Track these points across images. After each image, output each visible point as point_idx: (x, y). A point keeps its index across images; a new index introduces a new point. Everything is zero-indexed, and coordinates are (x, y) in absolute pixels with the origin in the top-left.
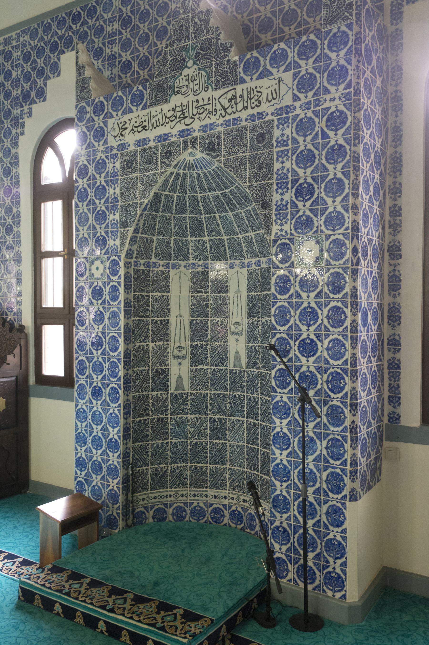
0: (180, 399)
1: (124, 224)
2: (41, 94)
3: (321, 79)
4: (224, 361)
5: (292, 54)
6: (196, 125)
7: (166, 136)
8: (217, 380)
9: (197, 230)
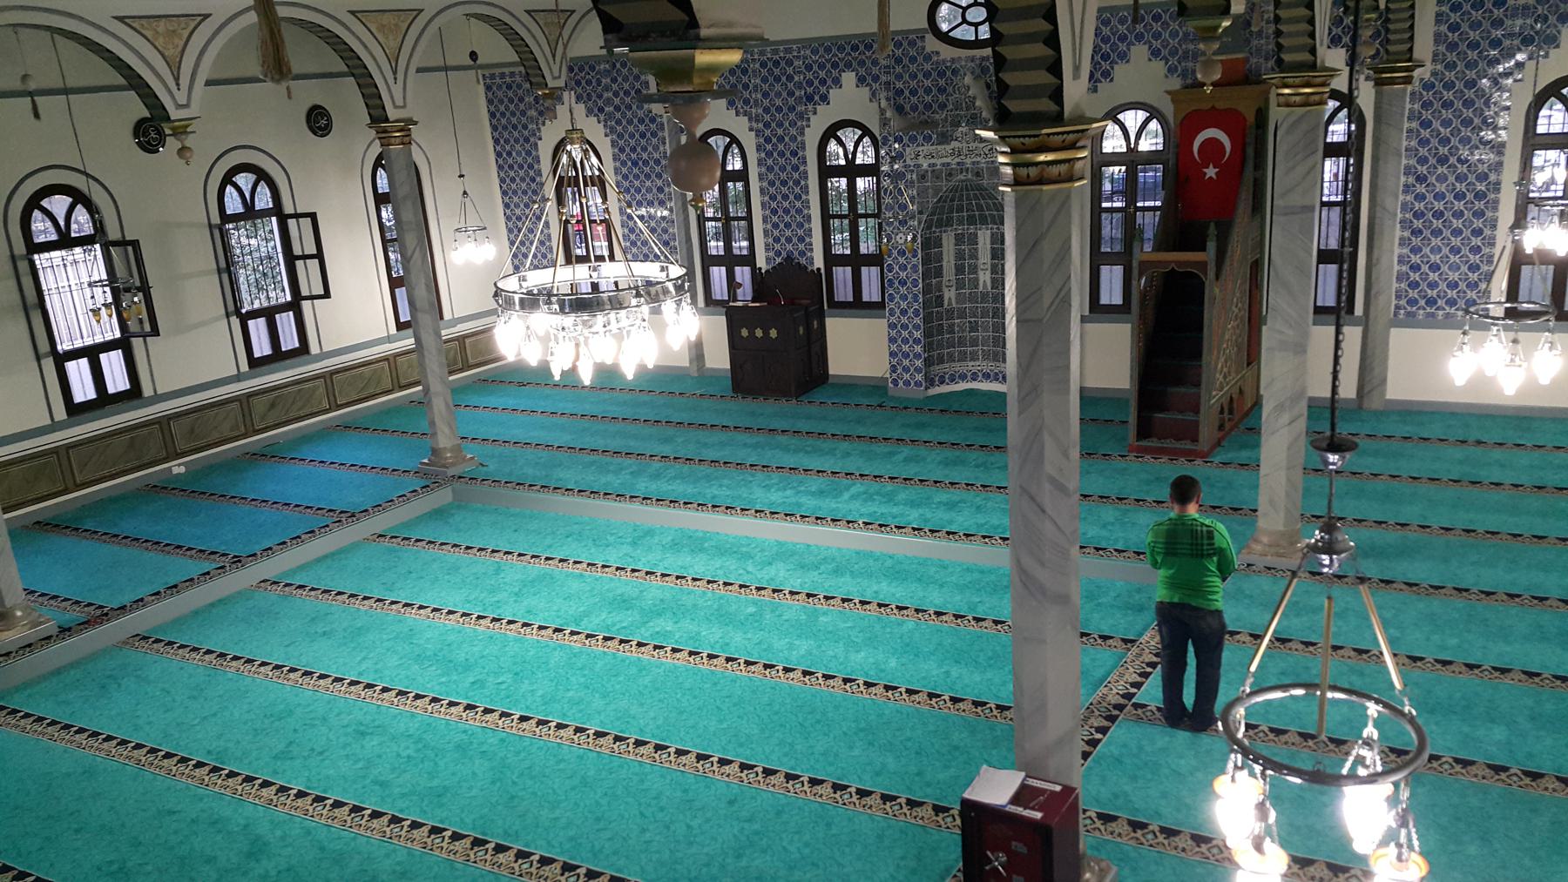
0: (950, 312)
1: (920, 213)
2: (825, 99)
6: (968, 161)
8: (972, 298)
9: (960, 209)
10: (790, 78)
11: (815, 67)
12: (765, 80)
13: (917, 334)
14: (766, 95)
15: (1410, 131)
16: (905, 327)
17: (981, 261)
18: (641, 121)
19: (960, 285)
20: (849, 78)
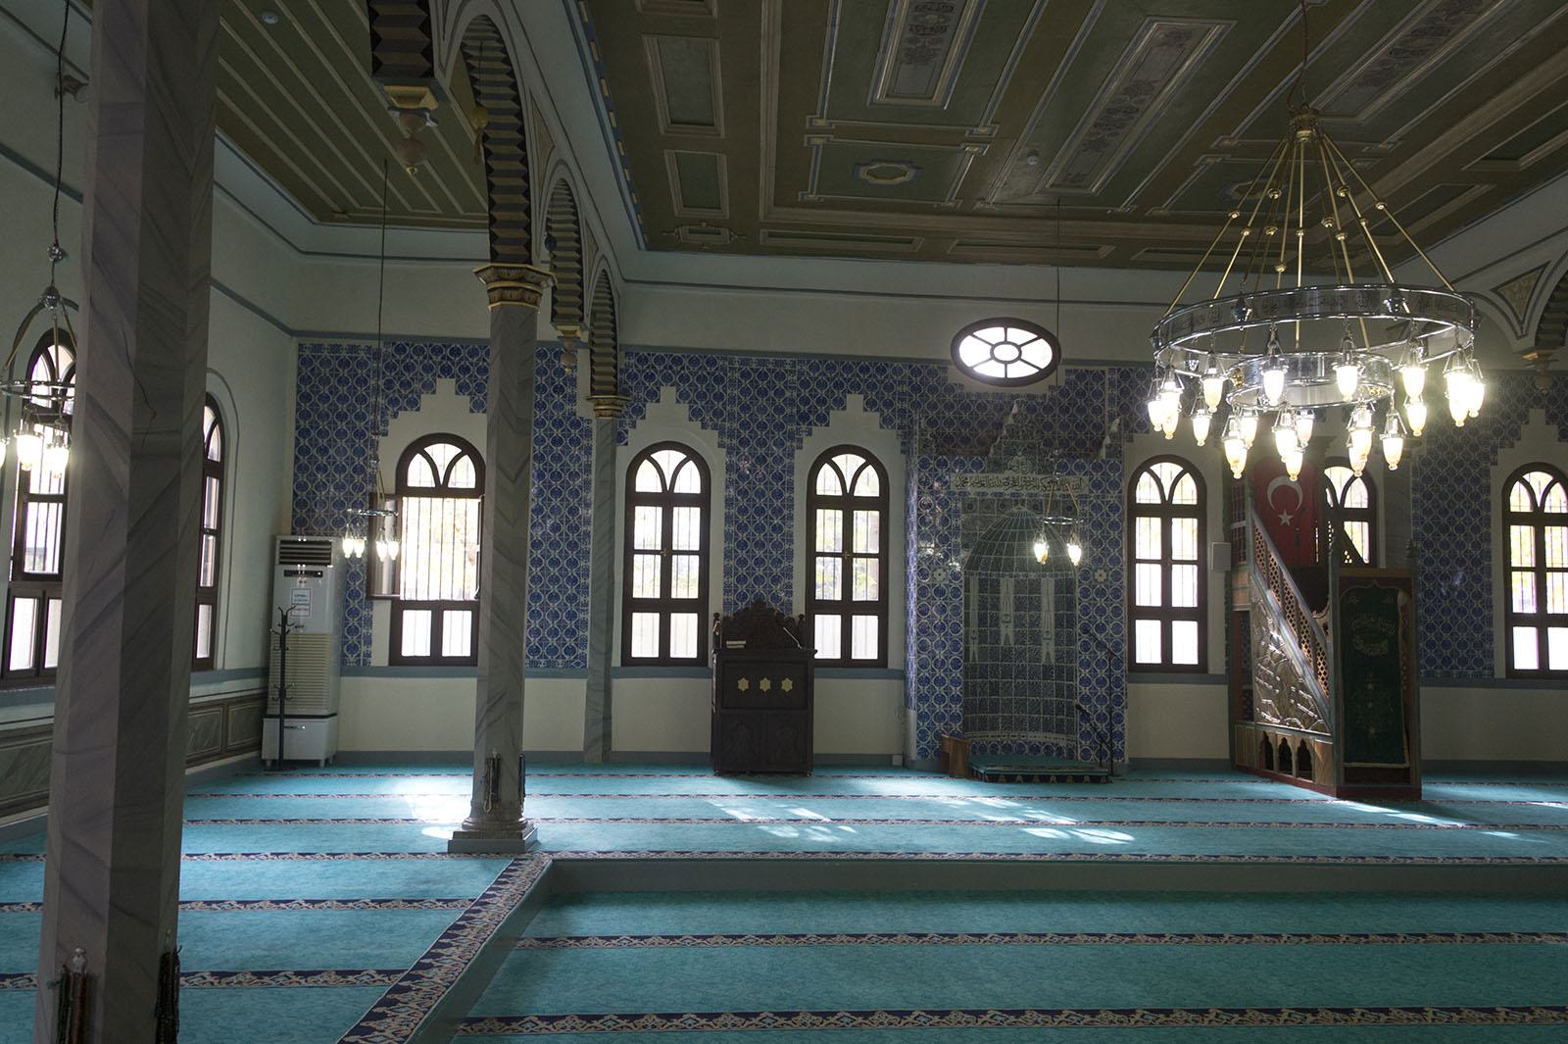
2: (823, 420)
3: (1105, 485)
4: (997, 641)
5: (1088, 467)
6: (1024, 492)
7: (1001, 494)
10: (780, 393)
11: (813, 385)
12: (745, 392)
13: (956, 691)
14: (745, 408)
15: (1415, 501)
16: (940, 681)
17: (1003, 612)
18: (558, 424)
19: (1019, 622)
20: (855, 401)
